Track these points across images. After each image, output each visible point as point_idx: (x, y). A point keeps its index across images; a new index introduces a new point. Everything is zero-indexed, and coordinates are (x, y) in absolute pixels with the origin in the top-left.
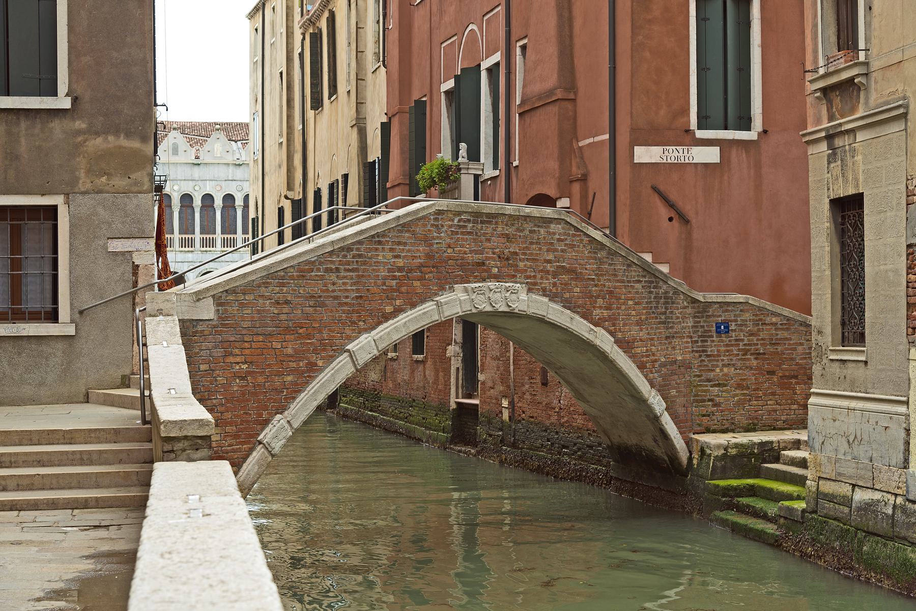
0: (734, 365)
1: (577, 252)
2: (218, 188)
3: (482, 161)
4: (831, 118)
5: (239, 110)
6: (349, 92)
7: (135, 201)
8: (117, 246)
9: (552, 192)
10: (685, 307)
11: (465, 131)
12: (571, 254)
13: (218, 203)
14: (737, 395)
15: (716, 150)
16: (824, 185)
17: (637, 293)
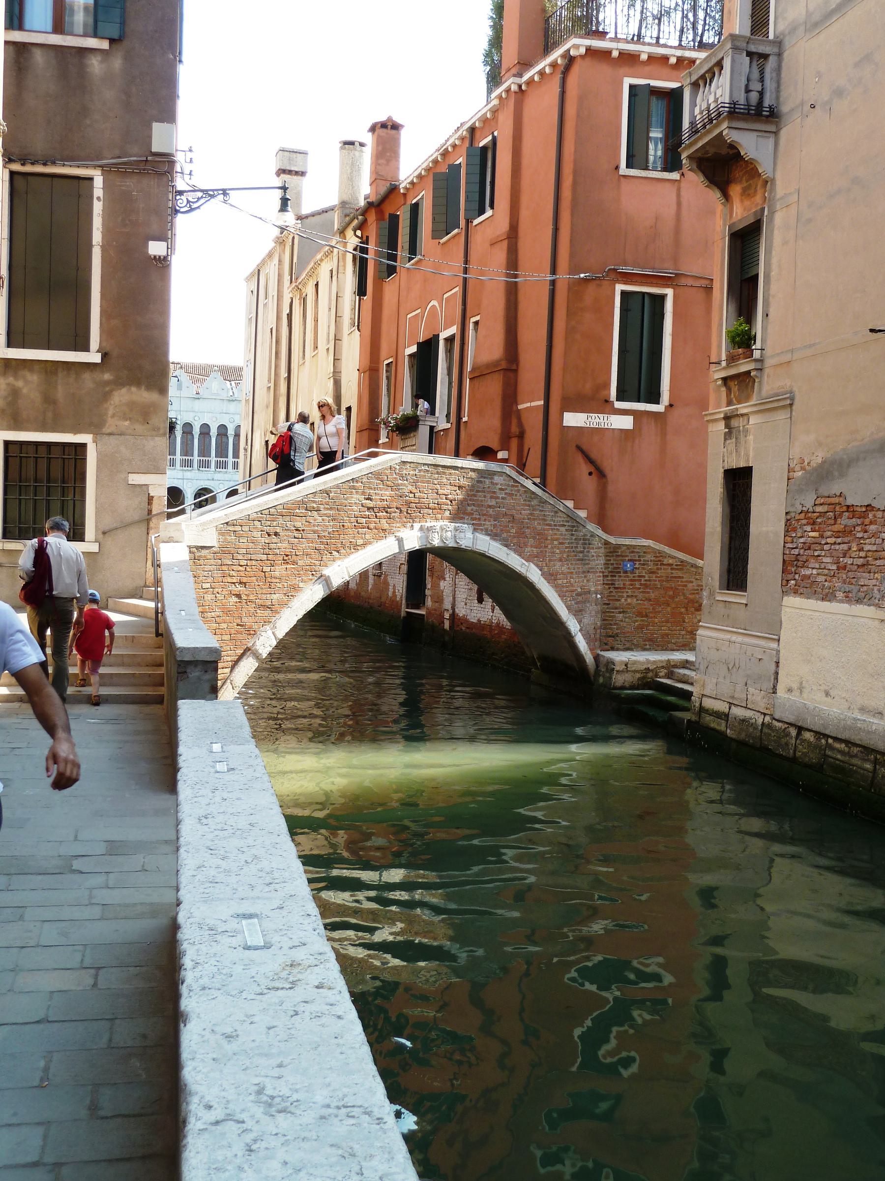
0: (636, 596)
1: (515, 499)
2: (214, 419)
3: (437, 414)
4: (729, 403)
5: (235, 354)
6: (328, 349)
7: (152, 443)
8: (136, 479)
9: (494, 444)
10: (599, 548)
11: (424, 388)
12: (510, 501)
13: (214, 432)
14: (637, 621)
15: (630, 419)
16: (719, 458)
17: (561, 535)
